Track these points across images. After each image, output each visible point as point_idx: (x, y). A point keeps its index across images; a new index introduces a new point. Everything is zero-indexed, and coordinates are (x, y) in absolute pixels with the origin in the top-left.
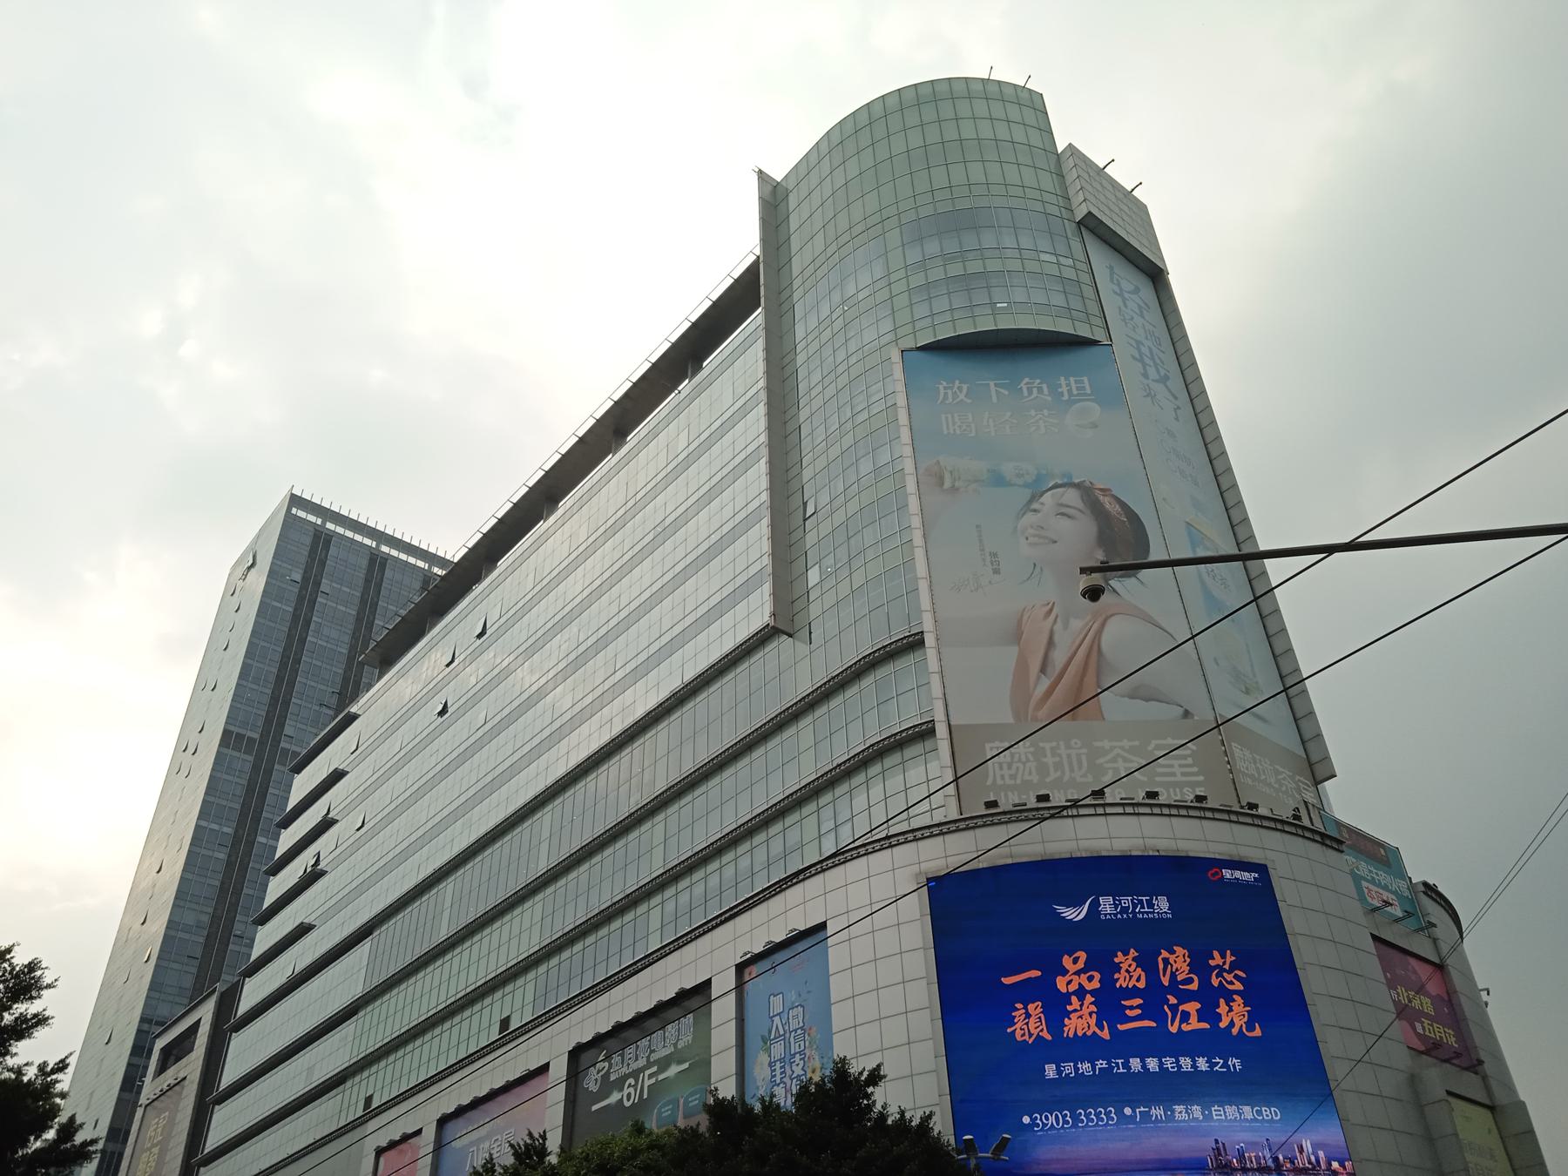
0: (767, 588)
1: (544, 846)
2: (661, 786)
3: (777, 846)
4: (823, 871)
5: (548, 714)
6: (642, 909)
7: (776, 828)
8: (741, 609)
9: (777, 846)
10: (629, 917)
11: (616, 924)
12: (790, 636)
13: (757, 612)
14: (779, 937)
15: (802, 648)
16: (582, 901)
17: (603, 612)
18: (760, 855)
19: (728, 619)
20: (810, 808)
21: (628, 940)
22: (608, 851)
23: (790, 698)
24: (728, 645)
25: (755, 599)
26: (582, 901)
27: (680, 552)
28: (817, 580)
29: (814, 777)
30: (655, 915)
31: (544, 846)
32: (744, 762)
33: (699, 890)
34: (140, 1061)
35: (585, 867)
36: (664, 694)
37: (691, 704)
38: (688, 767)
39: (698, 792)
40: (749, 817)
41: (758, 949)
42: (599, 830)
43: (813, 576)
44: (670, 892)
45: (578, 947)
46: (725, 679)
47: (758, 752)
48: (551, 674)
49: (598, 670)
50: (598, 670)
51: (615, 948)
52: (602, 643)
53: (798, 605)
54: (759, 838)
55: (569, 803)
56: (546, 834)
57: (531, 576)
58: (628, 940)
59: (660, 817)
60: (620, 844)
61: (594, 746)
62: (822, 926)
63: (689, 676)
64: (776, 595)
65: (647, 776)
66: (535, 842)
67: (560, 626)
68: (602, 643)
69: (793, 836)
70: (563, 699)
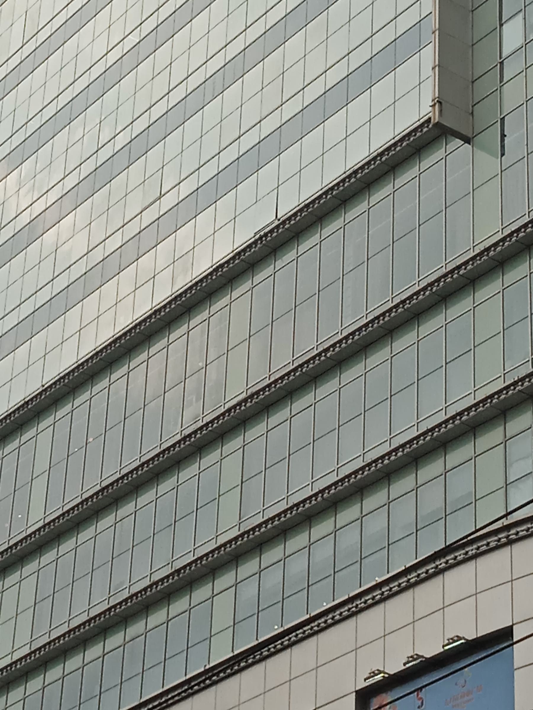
0: (429, 55)
1: (40, 485)
2: (236, 392)
3: (432, 500)
4: (510, 542)
5: (47, 267)
6: (202, 593)
7: (431, 469)
8: (382, 91)
9: (432, 500)
10: (179, 605)
11: (157, 617)
12: (467, 140)
13: (408, 99)
14: (431, 649)
15: (488, 163)
16: (101, 576)
17: (145, 91)
18: (404, 514)
19: (335, 125)
20: (493, 436)
21: (177, 644)
22: (146, 497)
23: (463, 250)
24: (358, 154)
25: (407, 72)
26: (101, 576)
27: (160, 86)
28: (520, 41)
29: (500, 385)
30: (223, 605)
31: (40, 485)
32: (378, 357)
33: (298, 566)
34: (503, 152)
35: (107, 521)
36: (244, 236)
37: (291, 255)
38: (283, 361)
39: (275, 419)
40: (386, 449)
41: (395, 667)
42: (131, 461)
43: (513, 35)
44: (250, 567)
45: (94, 651)
46: (351, 214)
47: (405, 341)
48: (53, 196)
49: (131, 195)
50: (131, 195)
51: (155, 656)
52: (137, 149)
53: (484, 87)
54: (403, 484)
55: (81, 414)
56: (42, 464)
57: (19, 26)
58: (177, 644)
59: (234, 444)
60: (166, 485)
61: (125, 321)
62: (503, 637)
63: (287, 207)
64: (443, 68)
65: (213, 372)
66: (24, 477)
67: (67, 115)
68: (137, 149)
69: (461, 484)
70: (72, 239)
